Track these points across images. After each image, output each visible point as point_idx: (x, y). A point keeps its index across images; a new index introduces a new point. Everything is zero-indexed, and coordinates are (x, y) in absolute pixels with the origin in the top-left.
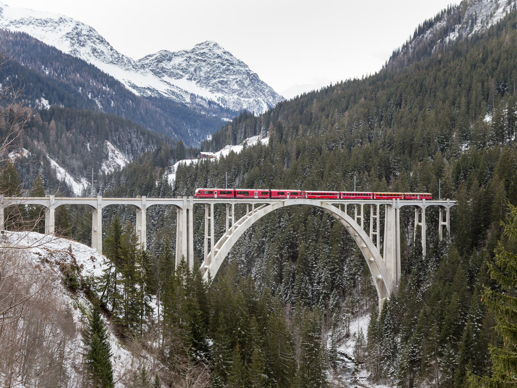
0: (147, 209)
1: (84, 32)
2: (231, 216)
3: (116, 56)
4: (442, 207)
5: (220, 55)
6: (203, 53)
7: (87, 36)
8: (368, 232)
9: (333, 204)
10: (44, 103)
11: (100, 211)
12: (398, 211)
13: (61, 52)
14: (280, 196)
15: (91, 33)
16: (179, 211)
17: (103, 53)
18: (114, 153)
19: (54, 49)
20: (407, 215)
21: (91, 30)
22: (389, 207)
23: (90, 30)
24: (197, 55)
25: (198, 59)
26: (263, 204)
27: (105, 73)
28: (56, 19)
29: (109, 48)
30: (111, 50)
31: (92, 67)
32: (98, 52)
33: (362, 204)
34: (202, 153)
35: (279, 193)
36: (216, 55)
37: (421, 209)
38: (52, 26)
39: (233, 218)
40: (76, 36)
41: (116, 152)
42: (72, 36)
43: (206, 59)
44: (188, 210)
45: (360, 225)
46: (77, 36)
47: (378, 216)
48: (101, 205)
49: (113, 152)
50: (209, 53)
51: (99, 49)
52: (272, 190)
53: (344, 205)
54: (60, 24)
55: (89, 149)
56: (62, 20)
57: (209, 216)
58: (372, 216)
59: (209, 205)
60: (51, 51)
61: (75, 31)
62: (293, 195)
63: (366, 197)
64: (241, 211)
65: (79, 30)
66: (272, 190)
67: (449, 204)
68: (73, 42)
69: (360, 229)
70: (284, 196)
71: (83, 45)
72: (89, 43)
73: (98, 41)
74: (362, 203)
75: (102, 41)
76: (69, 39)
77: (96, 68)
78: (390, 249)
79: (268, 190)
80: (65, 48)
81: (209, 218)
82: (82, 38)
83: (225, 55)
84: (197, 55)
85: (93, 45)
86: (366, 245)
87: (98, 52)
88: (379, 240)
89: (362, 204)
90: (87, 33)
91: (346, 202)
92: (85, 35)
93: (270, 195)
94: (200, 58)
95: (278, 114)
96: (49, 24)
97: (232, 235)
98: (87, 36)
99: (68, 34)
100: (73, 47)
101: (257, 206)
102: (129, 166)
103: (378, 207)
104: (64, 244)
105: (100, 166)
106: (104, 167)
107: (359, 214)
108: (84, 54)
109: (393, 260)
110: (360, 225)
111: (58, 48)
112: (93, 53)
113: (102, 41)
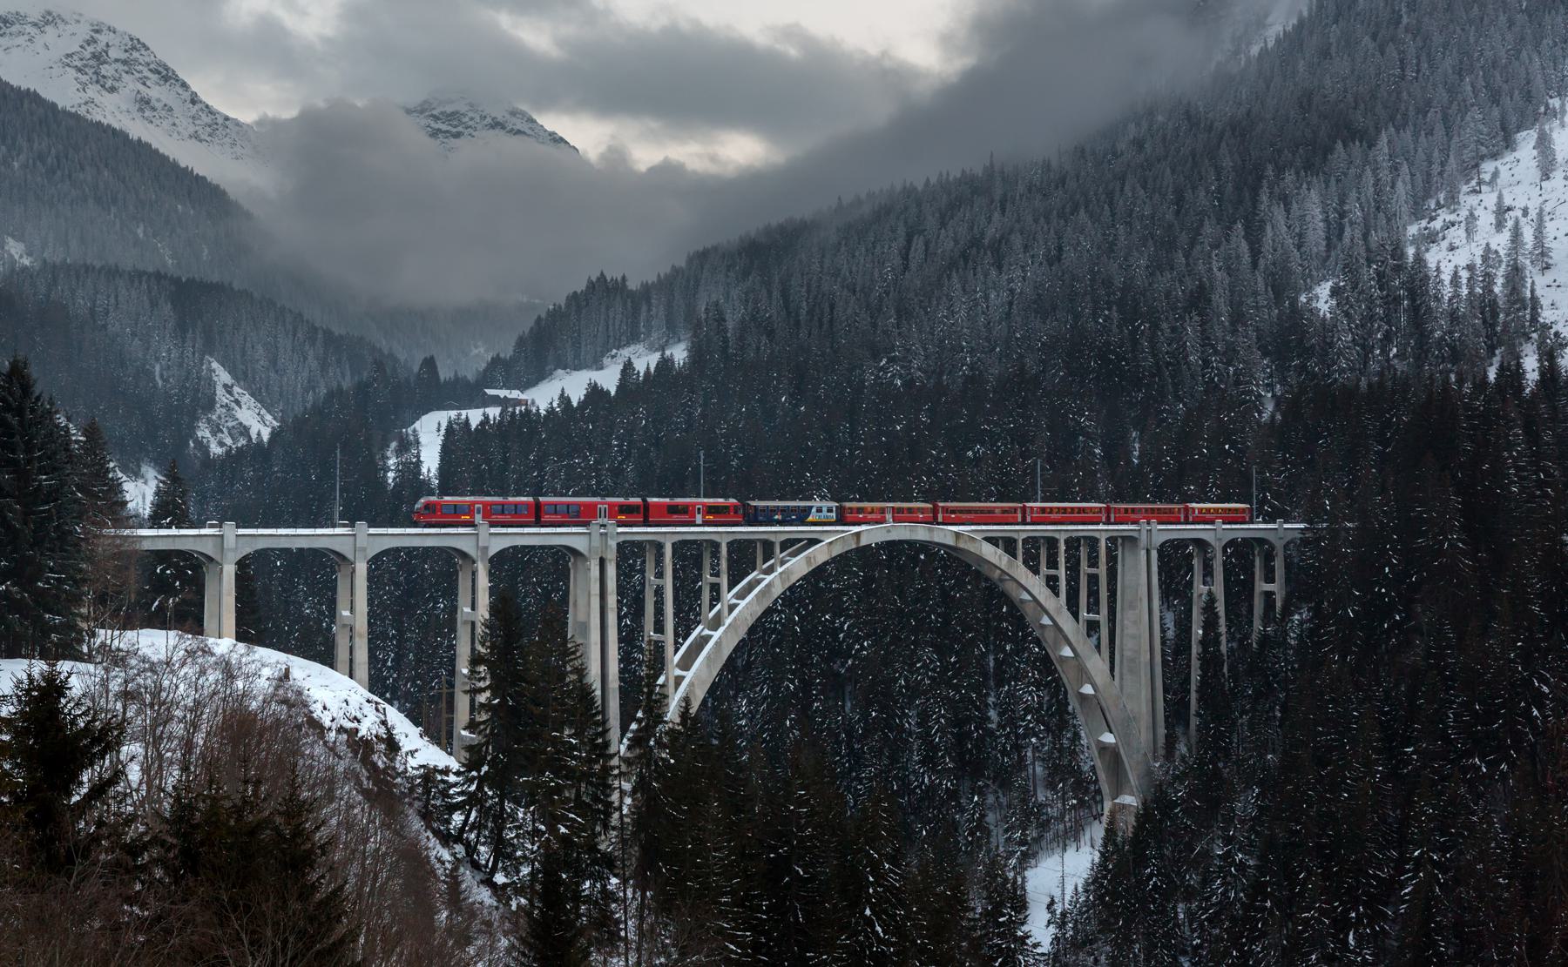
0: (491, 560)
1: (114, 53)
2: (717, 575)
3: (206, 119)
4: (1201, 544)
5: (500, 119)
6: (453, 114)
7: (125, 62)
8: (1076, 615)
9: (988, 539)
10: (13, 251)
11: (362, 569)
12: (1154, 554)
13: (54, 105)
14: (675, 518)
15: (136, 54)
16: (575, 564)
17: (171, 109)
18: (230, 393)
19: (33, 97)
20: (1175, 565)
21: (137, 45)
22: (1127, 545)
23: (134, 48)
24: (436, 118)
25: (439, 130)
26: (800, 540)
27: (183, 165)
28: (35, 16)
29: (186, 96)
30: (193, 102)
31: (142, 148)
32: (154, 109)
33: (1062, 538)
34: (490, 392)
35: (673, 509)
36: (489, 120)
37: (1272, 547)
38: (21, 33)
39: (724, 581)
40: (92, 62)
41: (236, 389)
42: (79, 64)
43: (460, 129)
44: (602, 562)
45: (1057, 595)
46: (94, 63)
47: (1102, 571)
48: (364, 549)
49: (228, 389)
50: (471, 114)
51: (158, 100)
52: (541, 499)
53: (1015, 541)
54: (48, 28)
55: (160, 383)
56: (49, 19)
57: (660, 575)
58: (1085, 568)
59: (715, 546)
60: (26, 105)
61: (90, 49)
62: (899, 516)
63: (681, 515)
64: (744, 559)
65: (100, 46)
66: (541, 499)
67: (1281, 533)
68: (84, 78)
69: (1055, 605)
70: (686, 518)
71: (113, 90)
72: (130, 85)
73: (154, 77)
74: (1062, 532)
75: (166, 79)
76: (72, 72)
77: (157, 151)
78: (1132, 660)
79: (639, 500)
80: (64, 92)
81: (714, 580)
82: (106, 70)
83: (514, 120)
84: (436, 118)
85: (142, 88)
86: (1073, 650)
87: (154, 109)
88: (1104, 634)
89: (1062, 538)
90: (124, 56)
91: (1020, 531)
92: (117, 60)
93: (646, 517)
94: (444, 127)
95: (697, 285)
96: (14, 29)
97: (722, 629)
98: (125, 62)
99: (68, 56)
100: (82, 94)
101: (785, 545)
102: (275, 434)
103: (1103, 544)
104: (267, 662)
105: (192, 429)
106: (203, 432)
107: (1053, 564)
108: (113, 111)
109: (1145, 693)
110: (1057, 595)
111: (48, 94)
112: (141, 110)
113: (166, 75)
